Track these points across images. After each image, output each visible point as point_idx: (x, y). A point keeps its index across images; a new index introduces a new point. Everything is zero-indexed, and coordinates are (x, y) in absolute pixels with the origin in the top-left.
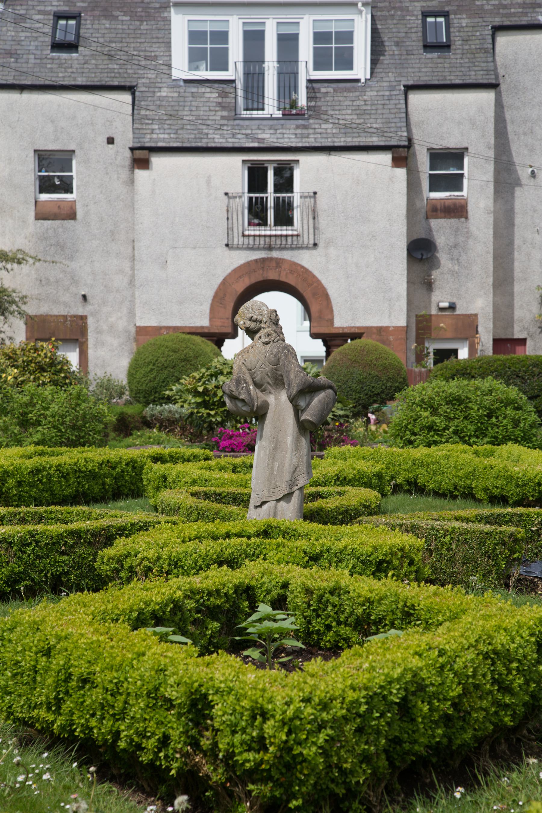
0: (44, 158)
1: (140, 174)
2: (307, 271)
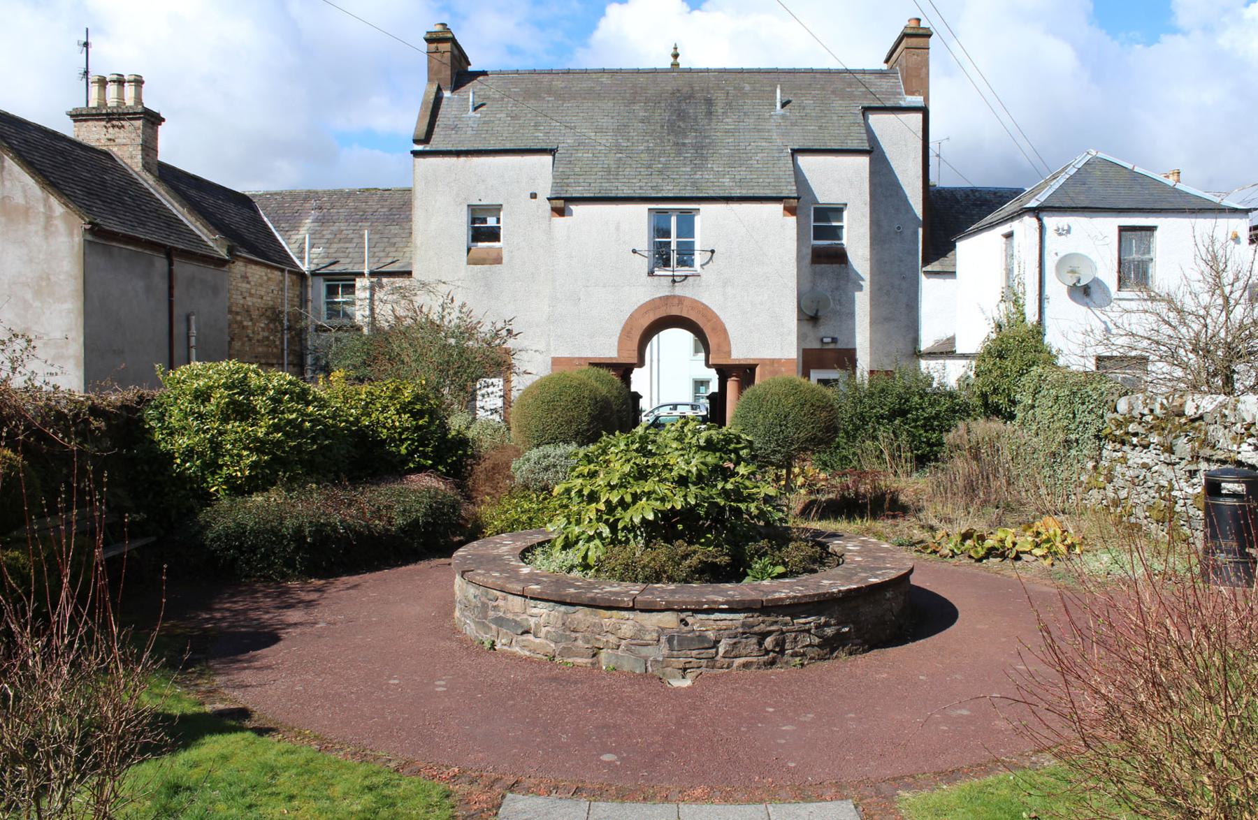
1: (558, 220)
2: (706, 307)
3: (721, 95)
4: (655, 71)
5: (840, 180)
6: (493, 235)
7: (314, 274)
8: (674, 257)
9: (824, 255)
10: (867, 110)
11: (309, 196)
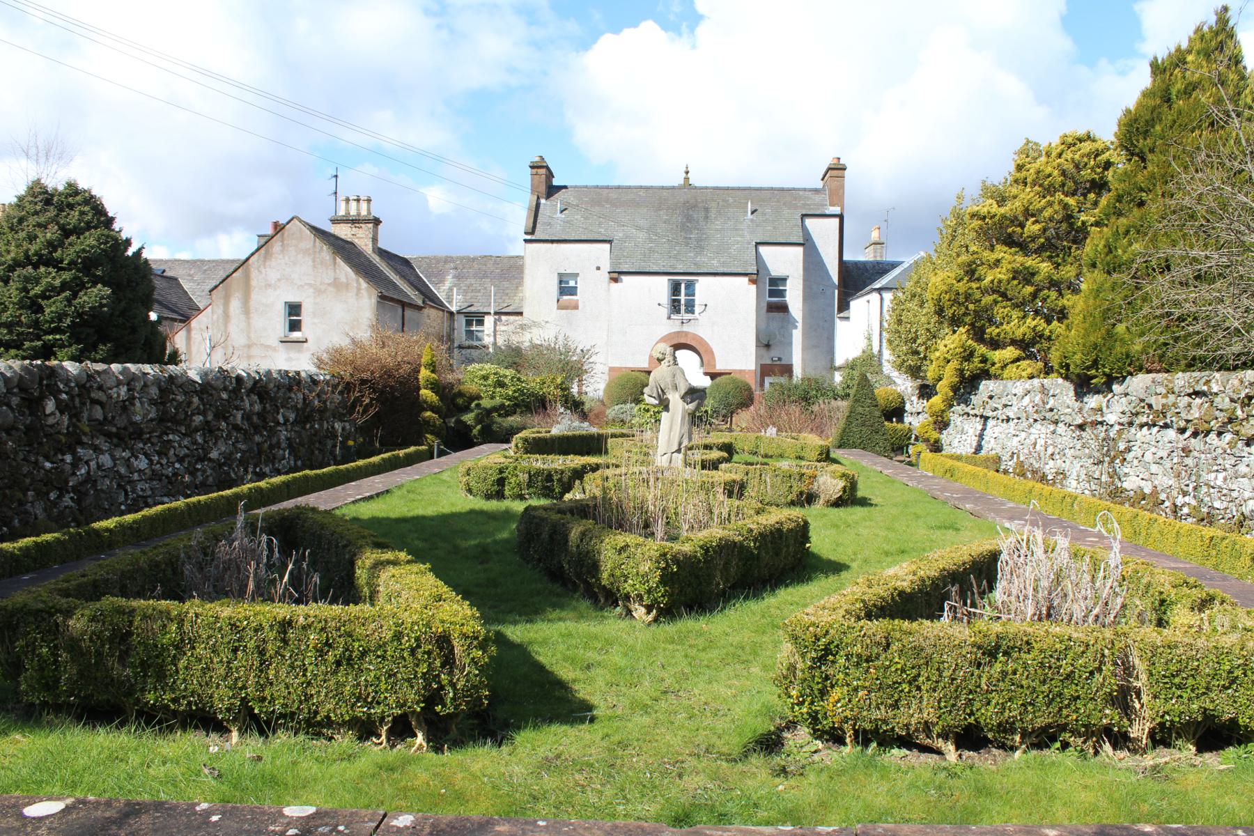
0: (562, 279)
1: (614, 285)
3: (714, 205)
4: (673, 188)
5: (785, 262)
6: (573, 291)
7: (459, 312)
8: (683, 308)
9: (775, 307)
10: (804, 216)
11: (447, 260)
